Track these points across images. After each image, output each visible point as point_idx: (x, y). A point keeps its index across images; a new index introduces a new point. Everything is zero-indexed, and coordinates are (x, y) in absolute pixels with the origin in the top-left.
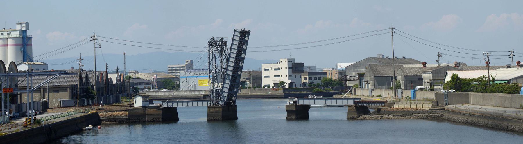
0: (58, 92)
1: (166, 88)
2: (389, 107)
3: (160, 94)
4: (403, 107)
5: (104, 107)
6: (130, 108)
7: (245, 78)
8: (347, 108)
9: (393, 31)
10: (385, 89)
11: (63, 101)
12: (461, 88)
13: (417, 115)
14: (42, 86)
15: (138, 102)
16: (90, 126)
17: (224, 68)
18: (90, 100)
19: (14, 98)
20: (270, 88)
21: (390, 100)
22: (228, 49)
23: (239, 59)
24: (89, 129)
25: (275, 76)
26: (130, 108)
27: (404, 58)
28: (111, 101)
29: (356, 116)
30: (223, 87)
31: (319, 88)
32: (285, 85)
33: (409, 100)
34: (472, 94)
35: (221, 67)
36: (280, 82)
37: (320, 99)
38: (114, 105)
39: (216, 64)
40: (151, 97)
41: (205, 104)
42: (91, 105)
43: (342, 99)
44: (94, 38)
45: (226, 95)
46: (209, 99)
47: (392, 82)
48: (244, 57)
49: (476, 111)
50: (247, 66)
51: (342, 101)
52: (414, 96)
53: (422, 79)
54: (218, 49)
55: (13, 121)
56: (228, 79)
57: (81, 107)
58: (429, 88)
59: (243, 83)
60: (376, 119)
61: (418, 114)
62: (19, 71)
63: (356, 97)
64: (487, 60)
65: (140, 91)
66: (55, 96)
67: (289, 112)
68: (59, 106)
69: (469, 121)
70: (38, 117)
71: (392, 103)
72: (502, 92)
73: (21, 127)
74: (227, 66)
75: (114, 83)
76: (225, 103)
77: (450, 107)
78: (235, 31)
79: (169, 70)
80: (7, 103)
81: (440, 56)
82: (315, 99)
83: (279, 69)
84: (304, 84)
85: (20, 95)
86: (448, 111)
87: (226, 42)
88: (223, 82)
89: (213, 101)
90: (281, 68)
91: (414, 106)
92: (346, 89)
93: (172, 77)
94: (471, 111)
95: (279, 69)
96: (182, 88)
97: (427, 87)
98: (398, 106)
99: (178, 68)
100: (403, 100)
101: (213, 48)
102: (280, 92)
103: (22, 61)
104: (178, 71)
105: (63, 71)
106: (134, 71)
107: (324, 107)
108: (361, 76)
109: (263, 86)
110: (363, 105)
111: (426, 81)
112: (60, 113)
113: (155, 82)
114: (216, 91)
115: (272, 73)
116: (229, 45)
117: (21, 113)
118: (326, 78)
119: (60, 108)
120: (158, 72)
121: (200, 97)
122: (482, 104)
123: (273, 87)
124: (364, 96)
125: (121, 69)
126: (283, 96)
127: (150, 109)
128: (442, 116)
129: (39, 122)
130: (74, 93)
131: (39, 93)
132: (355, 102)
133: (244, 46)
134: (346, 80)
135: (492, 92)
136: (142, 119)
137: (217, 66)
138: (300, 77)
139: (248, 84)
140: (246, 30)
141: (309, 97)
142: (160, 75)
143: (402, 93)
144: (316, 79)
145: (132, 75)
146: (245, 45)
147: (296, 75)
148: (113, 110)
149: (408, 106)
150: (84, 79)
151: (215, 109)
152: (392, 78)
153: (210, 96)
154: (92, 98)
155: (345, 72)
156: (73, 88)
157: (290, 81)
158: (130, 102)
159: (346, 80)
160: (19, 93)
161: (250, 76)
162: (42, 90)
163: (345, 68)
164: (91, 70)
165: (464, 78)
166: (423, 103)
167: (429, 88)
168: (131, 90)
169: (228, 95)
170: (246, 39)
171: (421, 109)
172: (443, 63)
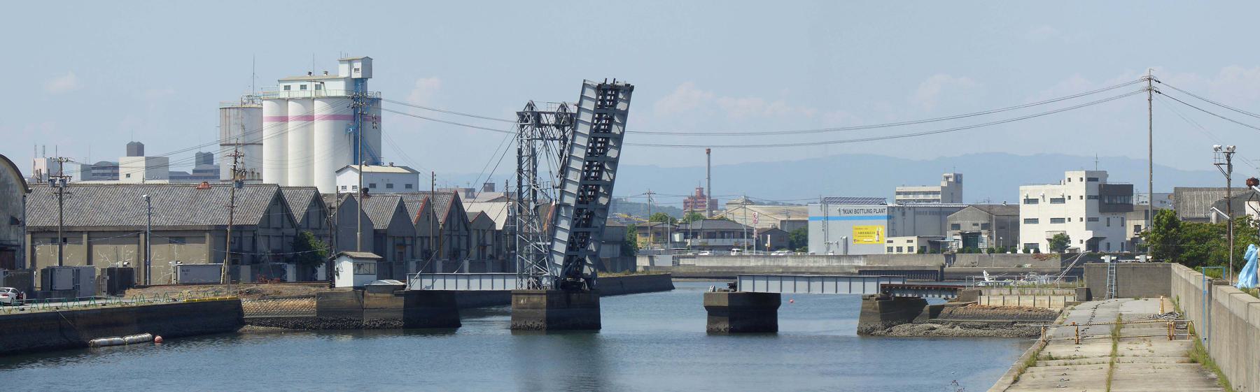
0: (184, 243)
2: (964, 303)
3: (768, 262)
4: (1000, 303)
7: (977, 225)
11: (185, 269)
12: (1182, 250)
13: (1025, 326)
25: (1054, 220)
39: (538, 178)
45: (559, 260)
48: (618, 158)
51: (864, 285)
56: (566, 218)
61: (1027, 324)
68: (174, 282)
75: (299, 221)
76: (556, 282)
83: (1062, 200)
90: (1069, 197)
95: (1062, 200)
96: (813, 247)
98: (1017, 301)
110: (905, 296)
115: (1044, 211)
119: (174, 285)
127: (373, 295)
131: (136, 246)
132: (883, 287)
138: (1123, 225)
139: (986, 242)
140: (621, 82)
147: (1108, 219)
148: (281, 295)
151: (529, 298)
157: (1089, 235)
161: (991, 218)
166: (1054, 293)
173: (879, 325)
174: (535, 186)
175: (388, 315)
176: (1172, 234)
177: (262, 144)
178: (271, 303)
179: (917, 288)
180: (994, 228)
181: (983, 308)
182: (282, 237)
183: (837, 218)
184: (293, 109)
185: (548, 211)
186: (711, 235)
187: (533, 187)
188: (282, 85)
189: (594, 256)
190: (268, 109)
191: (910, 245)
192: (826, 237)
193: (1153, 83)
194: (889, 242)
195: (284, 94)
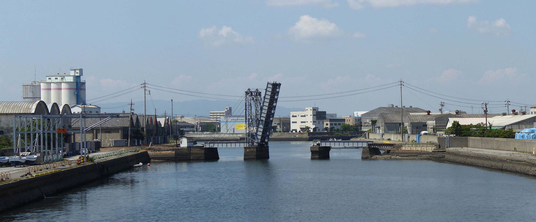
1: (208, 131)
3: (203, 136)
4: (409, 149)
5: (153, 147)
6: (177, 148)
8: (361, 150)
9: (401, 84)
10: (394, 133)
12: (461, 133)
14: (95, 127)
15: (184, 143)
16: (140, 163)
17: (258, 115)
18: (140, 141)
19: (67, 138)
20: (297, 132)
21: (398, 143)
22: (262, 99)
23: (272, 107)
24: (139, 166)
25: (302, 122)
26: (177, 148)
27: (411, 107)
28: (160, 142)
29: (369, 156)
30: (257, 131)
31: (339, 132)
32: (309, 130)
33: (414, 143)
34: (471, 139)
35: (256, 114)
36: (306, 127)
37: (339, 142)
38: (162, 145)
40: (195, 138)
41: (242, 145)
42: (141, 145)
43: (358, 142)
44: (144, 85)
45: (259, 137)
46: (245, 141)
47: (401, 127)
48: (276, 106)
49: (474, 153)
50: (278, 114)
52: (419, 140)
53: (426, 125)
54: (253, 98)
55: (66, 159)
56: (262, 124)
57: (132, 147)
58: (432, 133)
59: (275, 128)
60: (385, 159)
62: (72, 113)
63: (370, 140)
64: (485, 109)
65: (186, 133)
67: (313, 152)
69: (467, 161)
70: (91, 155)
71: (400, 146)
72: (498, 137)
73: (74, 164)
74: (261, 113)
75: (163, 126)
77: (451, 149)
78: (268, 83)
79: (211, 116)
80: (60, 142)
81: (442, 105)
82: (335, 142)
83: (305, 116)
84: (326, 129)
85: (74, 135)
86: (449, 153)
87: (260, 92)
88: (258, 127)
89: (249, 143)
90: (307, 115)
91: (419, 149)
92: (362, 133)
93: (214, 122)
94: (469, 153)
95: (305, 116)
97: (430, 132)
99: (219, 114)
100: (409, 143)
101: (249, 98)
102: (306, 136)
103: (76, 104)
104: (219, 117)
105: (115, 114)
106: (180, 116)
107: (343, 148)
108: (374, 122)
109: (291, 130)
111: (430, 127)
112: (112, 152)
113: (199, 126)
114: (251, 134)
115: (299, 119)
116: (263, 95)
117: (74, 151)
118: (345, 124)
119: (112, 147)
120: (201, 117)
121: (238, 139)
122: (504, 149)
123: (300, 131)
124: (376, 139)
125: (169, 113)
126: (308, 139)
128: (444, 157)
129: (92, 160)
130: (126, 134)
133: (276, 96)
134: (362, 126)
135: (488, 136)
137: (252, 113)
138: (323, 123)
140: (278, 82)
141: (330, 140)
142: (203, 120)
143: (409, 137)
144: (336, 125)
145: (179, 119)
146: (276, 95)
149: (414, 149)
150: (135, 121)
152: (400, 124)
153: (246, 138)
154: (143, 139)
155: (361, 119)
156: (124, 130)
157: (314, 126)
158: (177, 142)
159: (362, 126)
160: (72, 134)
161: (280, 122)
162: (95, 131)
163: (360, 116)
164: (141, 114)
165: (464, 124)
167: (432, 133)
168: (178, 132)
169: (262, 138)
170: (278, 90)
171: (425, 151)
172: (445, 112)
176: (459, 128)
177: (41, 98)
180: (282, 125)
183: (230, 122)
184: (53, 86)
188: (48, 78)
190: (43, 86)
193: (402, 83)
195: (48, 81)
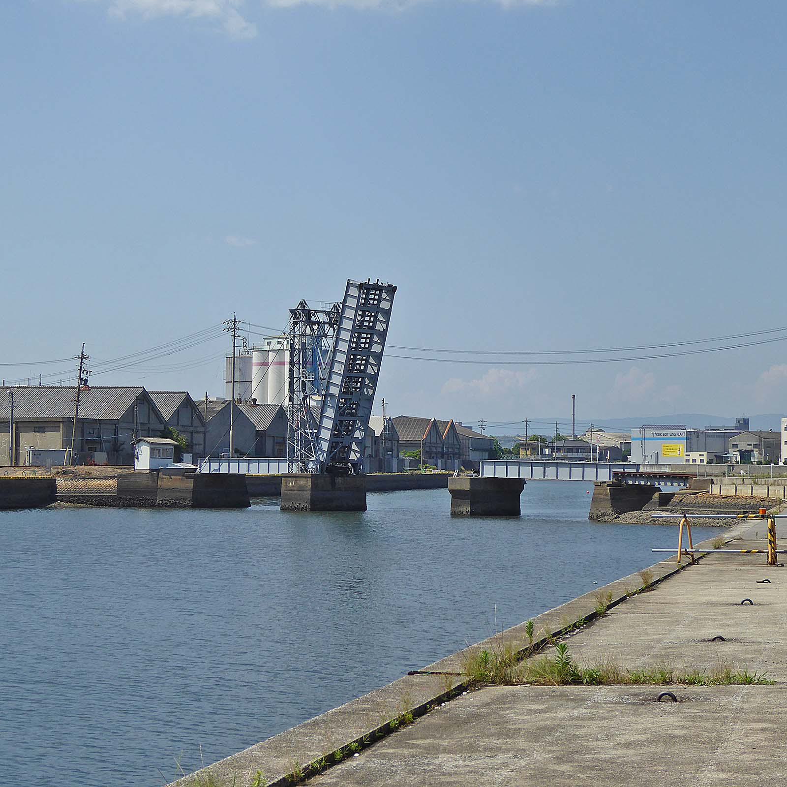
4: (732, 492)
44: (234, 326)
45: (325, 446)
66: (38, 441)
76: (321, 467)
110: (637, 483)
132: (616, 474)
136: (149, 500)
140: (384, 281)
173: (610, 511)
174: (303, 377)
175: (179, 495)
178: (81, 482)
179: (649, 476)
181: (714, 497)
182: (149, 431)
185: (428, 425)
186: (570, 450)
187: (302, 379)
188: (266, 341)
189: (359, 442)
190: (256, 357)
191: (702, 458)
192: (644, 452)
194: (686, 455)
195: (267, 348)
